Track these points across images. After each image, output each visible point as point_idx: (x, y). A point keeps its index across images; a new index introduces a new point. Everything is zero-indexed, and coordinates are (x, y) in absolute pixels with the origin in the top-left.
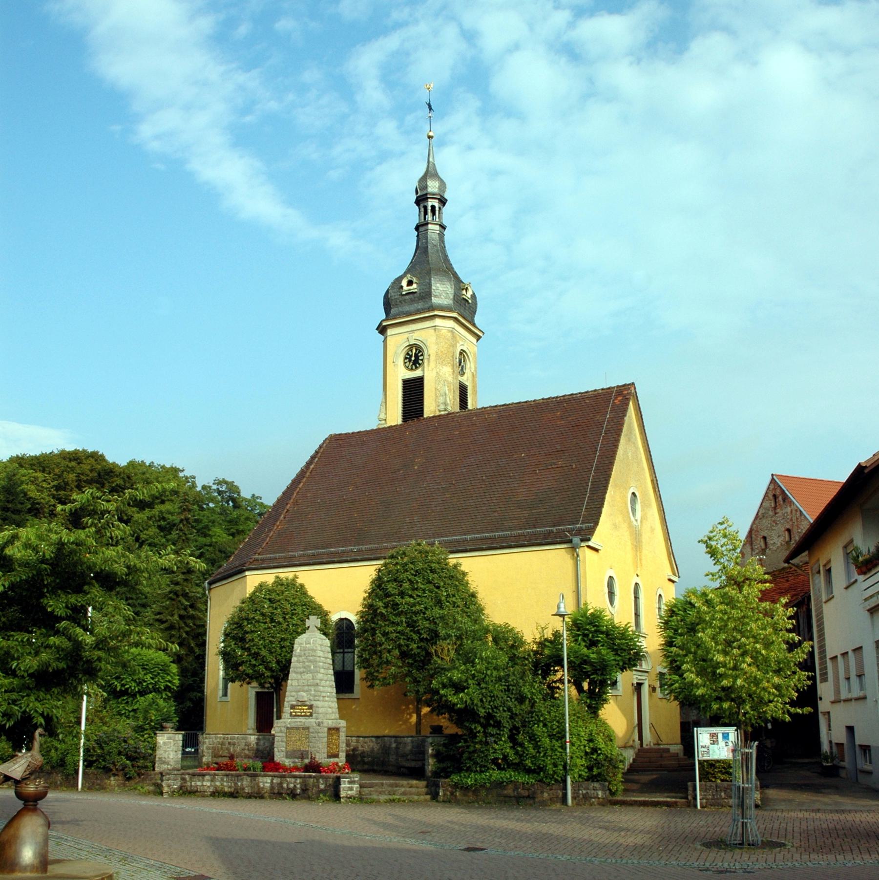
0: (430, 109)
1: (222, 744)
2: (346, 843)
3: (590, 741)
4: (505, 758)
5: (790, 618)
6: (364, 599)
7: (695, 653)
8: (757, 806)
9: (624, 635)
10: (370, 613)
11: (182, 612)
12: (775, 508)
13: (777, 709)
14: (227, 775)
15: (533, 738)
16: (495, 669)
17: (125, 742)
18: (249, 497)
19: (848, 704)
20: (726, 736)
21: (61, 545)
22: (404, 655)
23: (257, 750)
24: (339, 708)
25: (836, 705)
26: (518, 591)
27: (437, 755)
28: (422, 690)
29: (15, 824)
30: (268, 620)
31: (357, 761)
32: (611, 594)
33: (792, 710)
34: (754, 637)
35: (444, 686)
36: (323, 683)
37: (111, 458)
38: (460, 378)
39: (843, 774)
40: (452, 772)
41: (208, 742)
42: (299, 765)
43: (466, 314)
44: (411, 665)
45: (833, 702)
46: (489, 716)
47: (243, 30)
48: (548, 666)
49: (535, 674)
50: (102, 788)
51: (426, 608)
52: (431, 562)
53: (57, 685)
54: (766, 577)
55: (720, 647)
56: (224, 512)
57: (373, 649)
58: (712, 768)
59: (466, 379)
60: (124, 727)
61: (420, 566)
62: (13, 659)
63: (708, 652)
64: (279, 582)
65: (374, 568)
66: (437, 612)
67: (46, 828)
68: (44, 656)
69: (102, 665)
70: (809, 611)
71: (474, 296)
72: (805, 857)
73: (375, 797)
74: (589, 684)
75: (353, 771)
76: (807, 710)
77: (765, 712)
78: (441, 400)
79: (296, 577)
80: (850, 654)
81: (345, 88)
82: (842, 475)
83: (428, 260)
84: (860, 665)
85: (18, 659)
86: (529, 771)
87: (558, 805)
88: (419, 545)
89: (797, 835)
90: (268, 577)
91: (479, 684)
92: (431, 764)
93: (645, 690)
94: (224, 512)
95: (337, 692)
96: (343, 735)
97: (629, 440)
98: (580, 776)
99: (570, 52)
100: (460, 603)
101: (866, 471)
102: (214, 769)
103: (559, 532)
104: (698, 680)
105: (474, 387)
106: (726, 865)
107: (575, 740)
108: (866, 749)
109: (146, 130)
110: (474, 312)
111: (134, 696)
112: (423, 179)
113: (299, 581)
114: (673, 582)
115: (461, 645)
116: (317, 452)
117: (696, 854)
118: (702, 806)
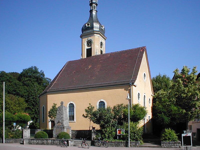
43: (102, 33)
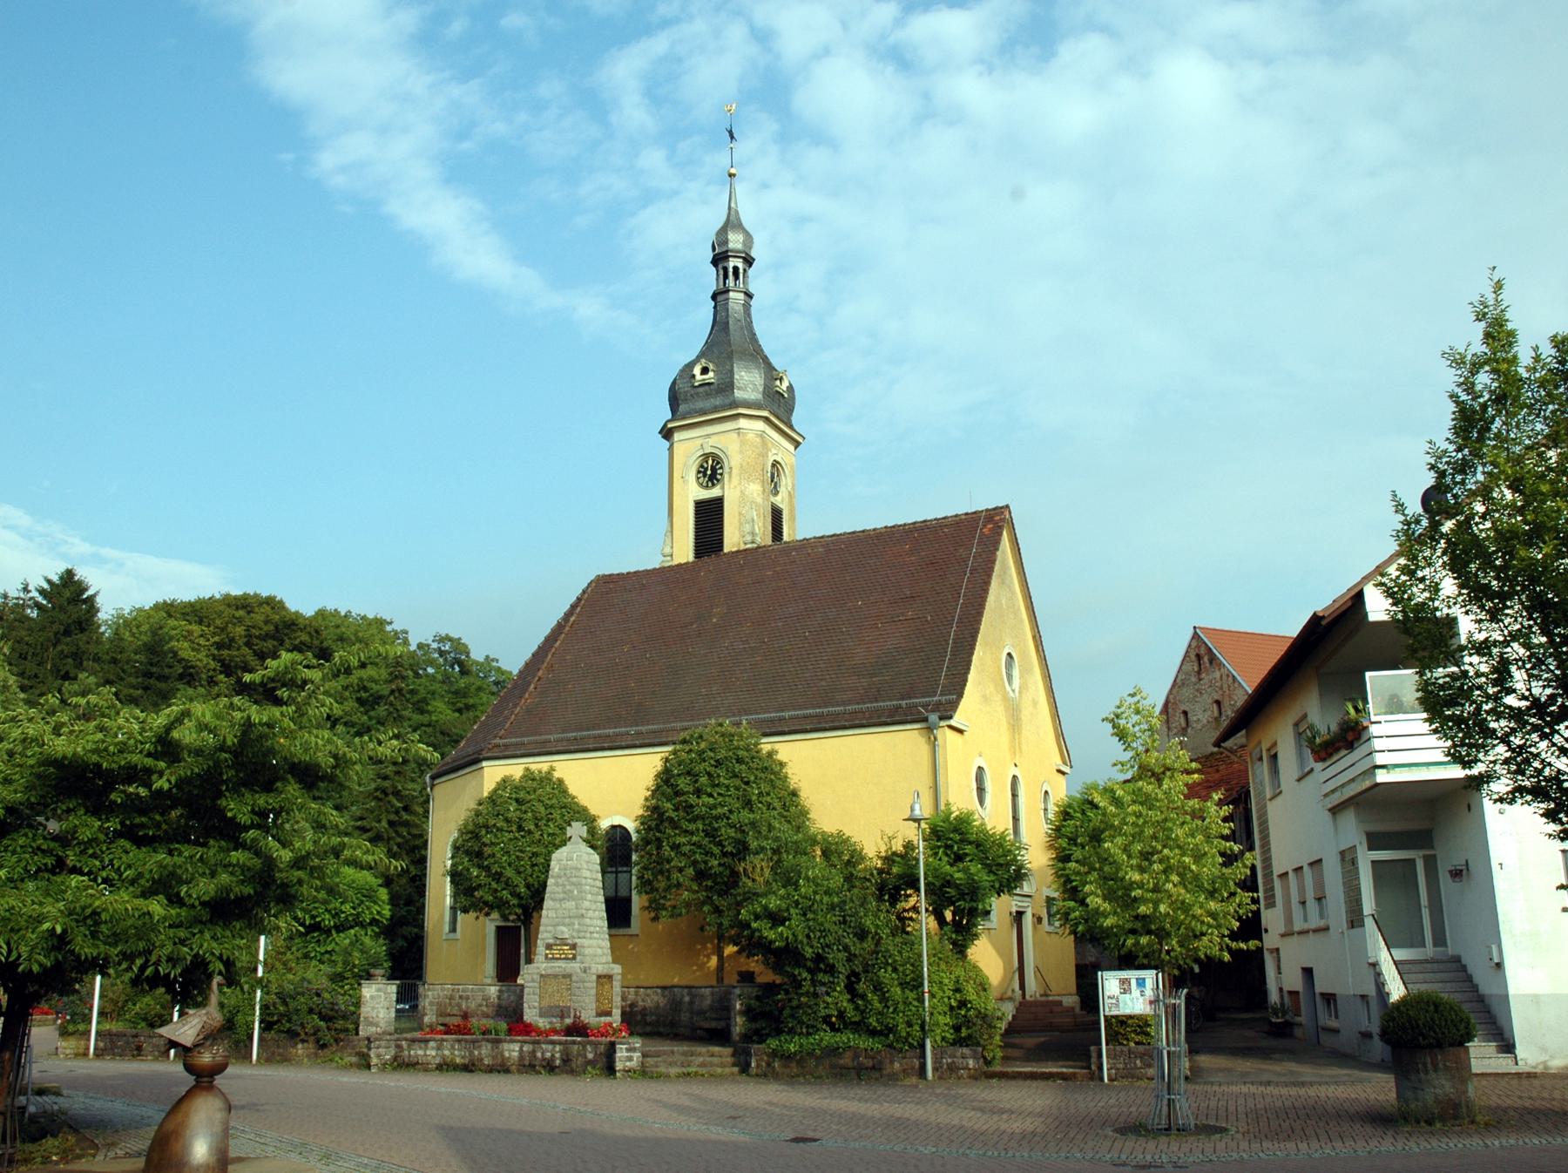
0: (732, 137)
1: (452, 998)
2: (627, 1132)
3: (957, 990)
4: (841, 1015)
5: (1225, 820)
6: (646, 799)
7: (1101, 869)
8: (1187, 1078)
9: (1000, 842)
10: (655, 819)
11: (393, 817)
12: (1199, 672)
13: (1212, 945)
14: (459, 1041)
15: (878, 987)
16: (826, 893)
17: (318, 995)
18: (481, 659)
19: (1303, 937)
20: (1141, 983)
21: (248, 725)
22: (701, 875)
23: (500, 1006)
24: (612, 948)
25: (1288, 939)
26: (854, 788)
27: (748, 1012)
28: (726, 923)
29: (184, 1107)
30: (514, 828)
31: (637, 1021)
32: (981, 790)
33: (1234, 945)
34: (1179, 847)
35: (757, 917)
36: (590, 914)
37: (292, 605)
38: (773, 499)
39: (1298, 1032)
40: (768, 1035)
41: (431, 995)
42: (558, 1026)
43: (781, 412)
44: (708, 889)
45: (1283, 936)
46: (819, 958)
47: (458, 27)
48: (897, 889)
49: (880, 899)
50: (285, 1060)
51: (731, 811)
52: (738, 748)
53: (239, 917)
54: (1194, 765)
55: (1134, 862)
56: (447, 680)
57: (658, 867)
58: (1123, 1026)
59: (780, 500)
60: (317, 975)
61: (722, 754)
62: (181, 882)
63: (1118, 869)
64: (529, 775)
65: (659, 756)
66: (746, 816)
67: (224, 1114)
68: (224, 878)
69: (304, 890)
70: (1248, 812)
71: (790, 388)
72: (1256, 1146)
73: (663, 1070)
74: (954, 914)
75: (631, 1034)
76: (1253, 944)
77: (1197, 949)
78: (748, 528)
79: (552, 769)
80: (1306, 868)
81: (596, 105)
82: (1293, 627)
83: (729, 339)
84: (1319, 883)
85: (188, 882)
86: (873, 1033)
87: (914, 1080)
88: (721, 725)
89: (1242, 1116)
90: (514, 769)
91: (804, 914)
92: (739, 1025)
93: (1028, 920)
94: (447, 680)
95: (610, 927)
96: (617, 985)
97: (1003, 582)
98: (943, 1039)
99: (897, 58)
100: (777, 804)
101: (1324, 623)
102: (440, 1032)
103: (909, 707)
104: (1106, 906)
105: (792, 511)
106: (1148, 1157)
107: (935, 989)
108: (1329, 998)
109: (327, 160)
110: (790, 410)
111: (328, 932)
112: (723, 231)
113: (557, 775)
114: (1063, 773)
115: (779, 861)
116: (579, 599)
117: (1108, 1144)
118: (1110, 1079)
